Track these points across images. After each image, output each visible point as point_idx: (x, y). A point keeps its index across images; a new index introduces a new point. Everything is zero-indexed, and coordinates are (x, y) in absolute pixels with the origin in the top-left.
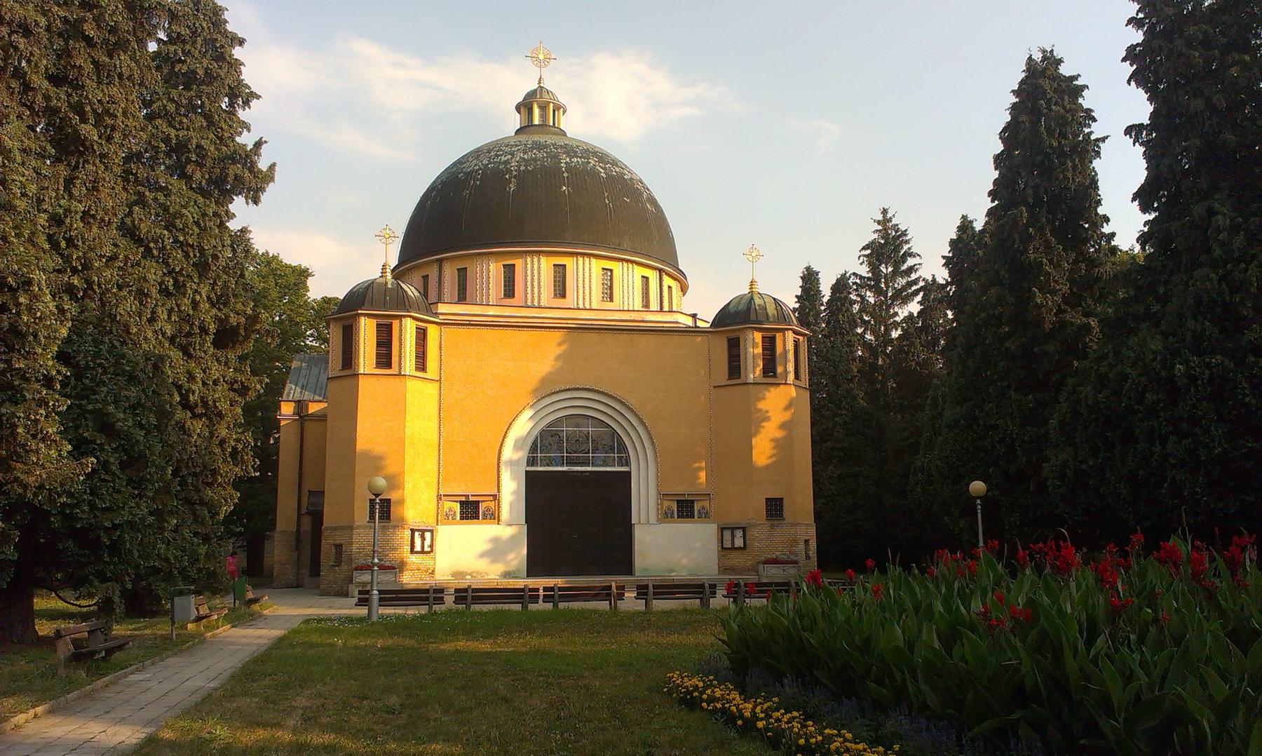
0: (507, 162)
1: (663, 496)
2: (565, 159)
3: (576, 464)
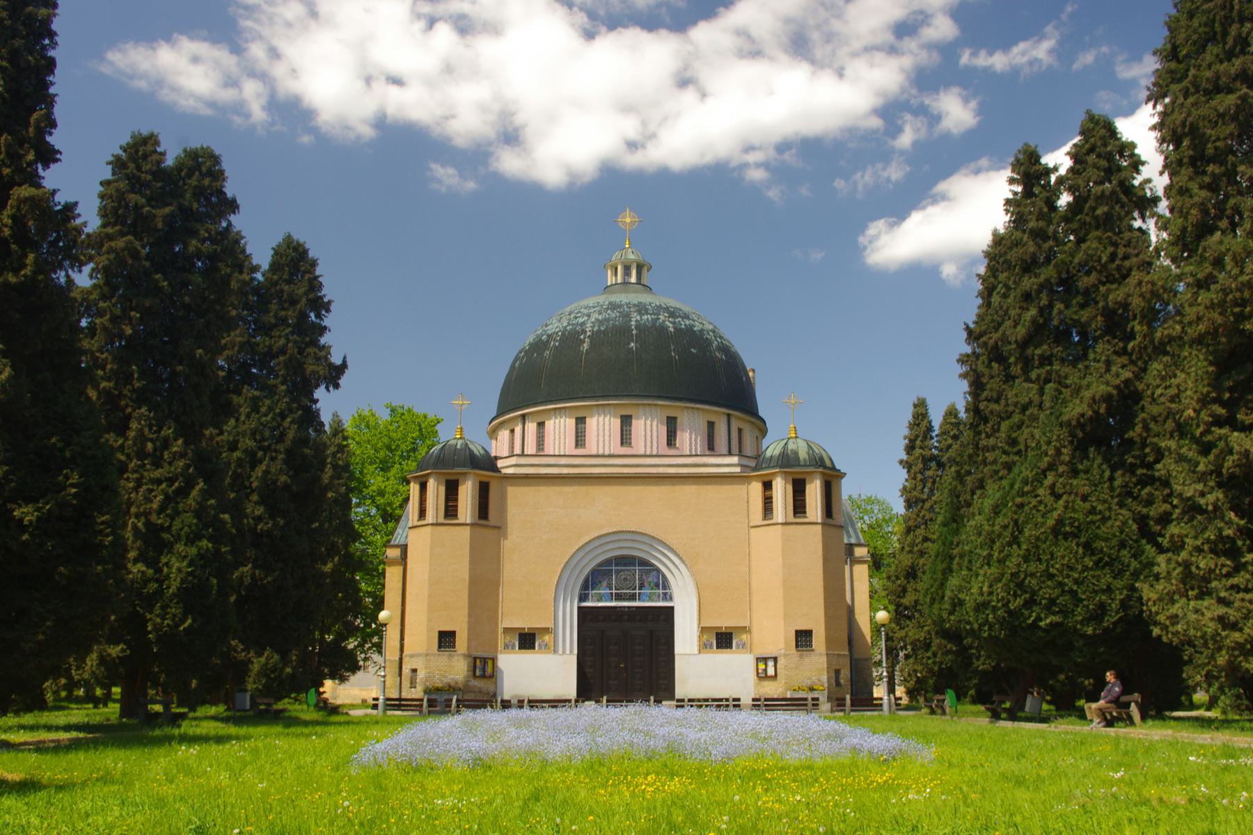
0: (583, 324)
1: (703, 630)
2: (635, 317)
3: (625, 600)
